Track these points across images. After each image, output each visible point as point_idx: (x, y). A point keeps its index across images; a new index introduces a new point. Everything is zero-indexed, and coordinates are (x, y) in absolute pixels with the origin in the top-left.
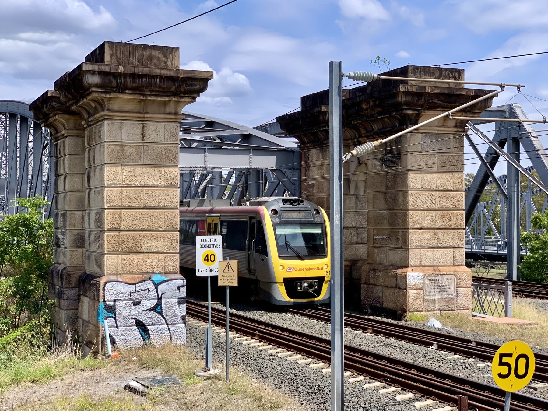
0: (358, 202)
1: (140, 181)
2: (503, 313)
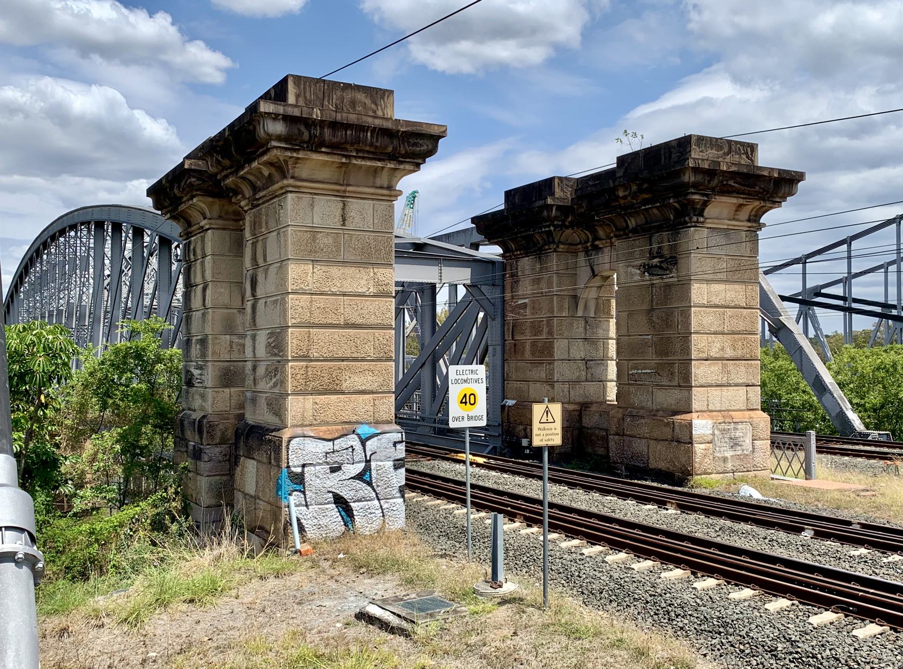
0: (588, 327)
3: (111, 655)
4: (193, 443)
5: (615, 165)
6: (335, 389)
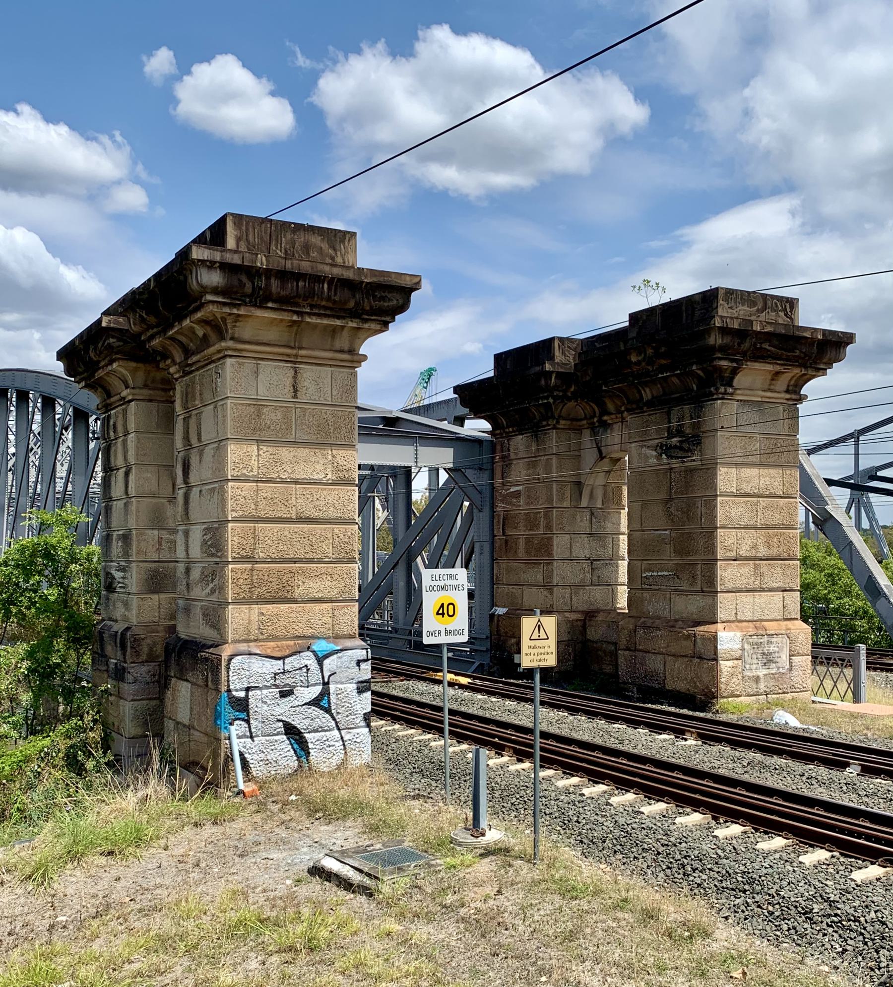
1: (290, 471)
2: (850, 694)
3: (13, 920)
4: (115, 661)
5: (627, 324)
6: (286, 597)
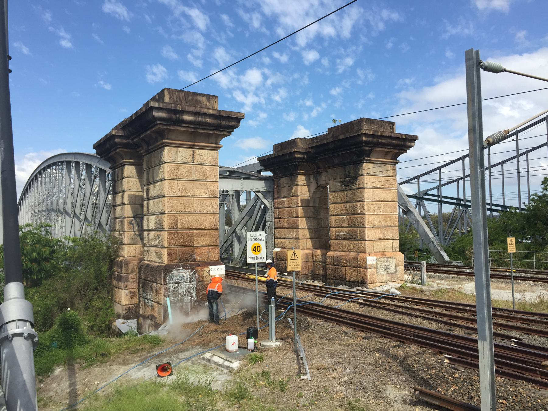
5: (327, 133)
